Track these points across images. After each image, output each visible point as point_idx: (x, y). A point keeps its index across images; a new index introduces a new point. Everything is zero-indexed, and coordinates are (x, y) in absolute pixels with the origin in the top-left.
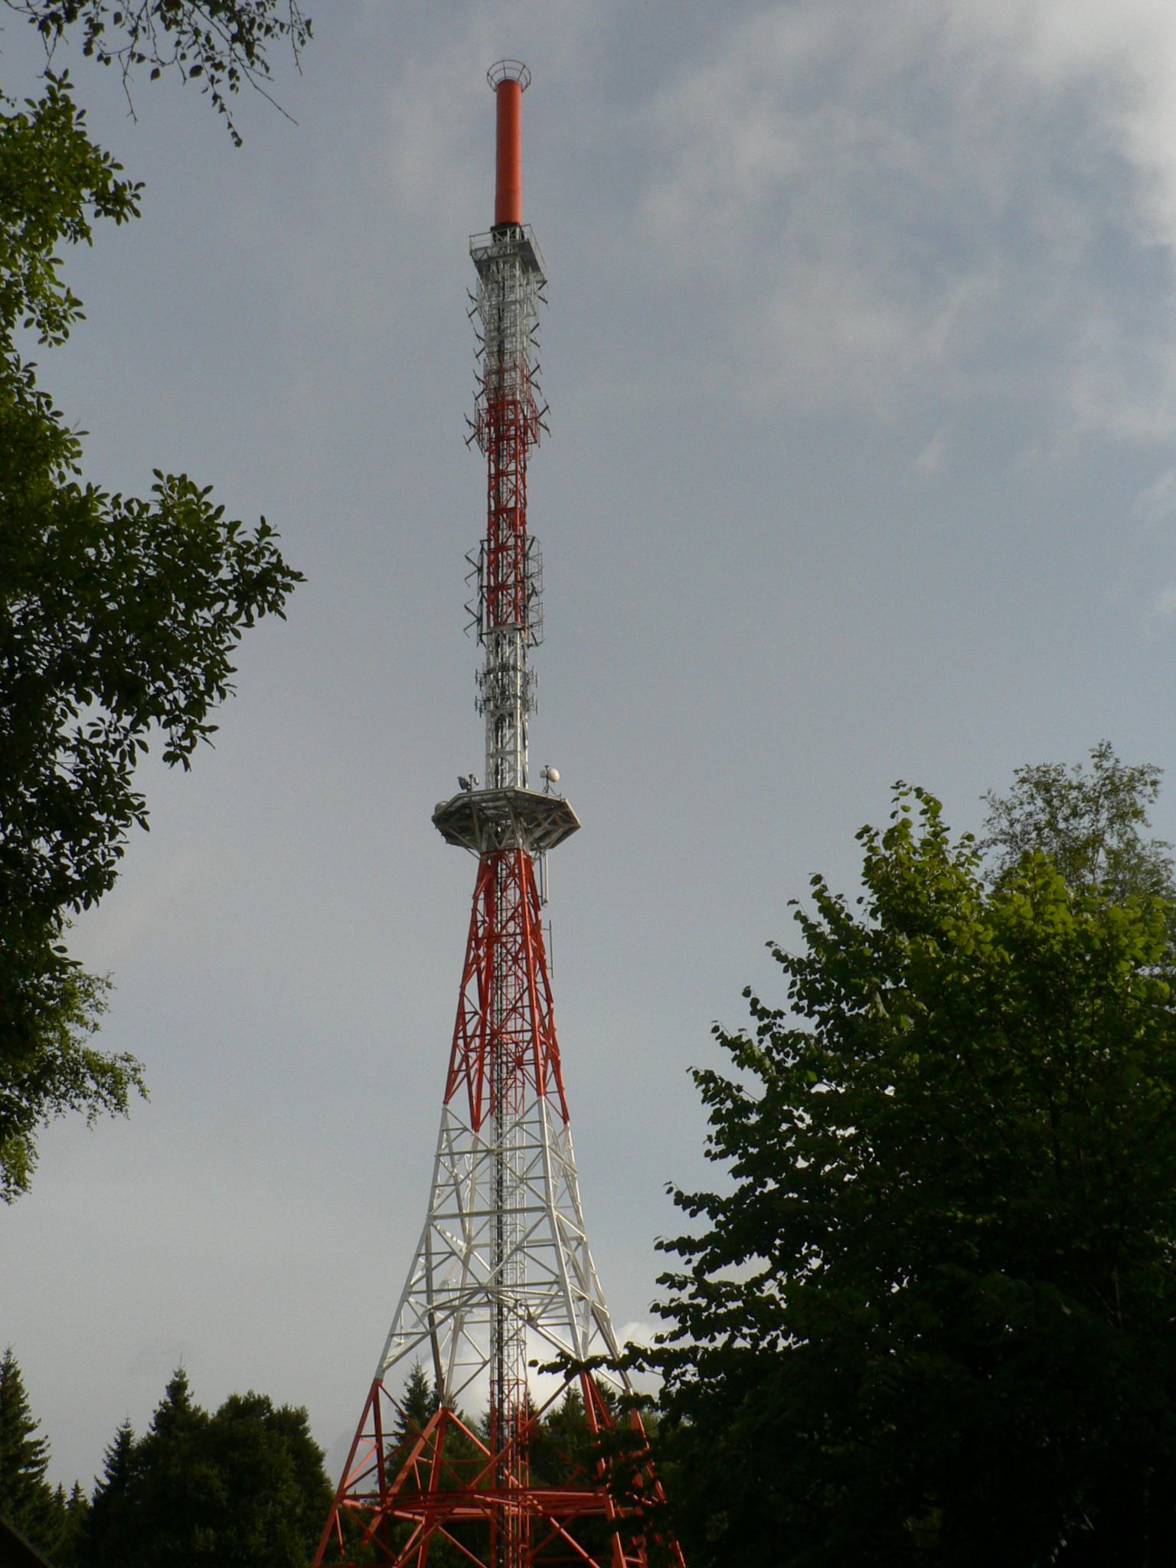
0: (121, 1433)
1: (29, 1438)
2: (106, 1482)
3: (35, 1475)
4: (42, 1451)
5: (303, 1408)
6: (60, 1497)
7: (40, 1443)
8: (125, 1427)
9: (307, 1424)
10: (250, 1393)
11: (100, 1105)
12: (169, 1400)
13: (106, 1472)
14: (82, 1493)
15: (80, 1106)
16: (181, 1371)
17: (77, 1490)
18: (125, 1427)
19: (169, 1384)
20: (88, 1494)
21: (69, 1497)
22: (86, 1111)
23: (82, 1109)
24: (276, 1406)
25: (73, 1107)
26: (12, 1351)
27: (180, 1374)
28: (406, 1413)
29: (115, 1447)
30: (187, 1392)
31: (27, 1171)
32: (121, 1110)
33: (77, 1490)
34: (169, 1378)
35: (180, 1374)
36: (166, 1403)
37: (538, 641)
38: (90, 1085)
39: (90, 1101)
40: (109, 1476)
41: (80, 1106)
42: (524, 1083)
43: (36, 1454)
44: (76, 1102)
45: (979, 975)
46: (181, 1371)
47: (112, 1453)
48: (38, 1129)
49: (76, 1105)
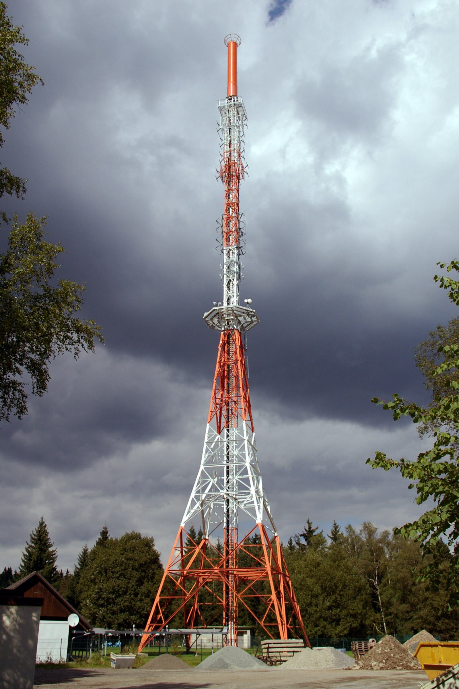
0: (84, 549)
1: (51, 549)
2: (79, 567)
3: (52, 562)
4: (54, 554)
5: (152, 537)
6: (62, 574)
7: (54, 551)
8: (85, 547)
9: (154, 543)
10: (133, 532)
11: (80, 348)
12: (101, 537)
13: (79, 563)
14: (69, 573)
15: (71, 349)
16: (105, 527)
17: (68, 572)
18: (85, 547)
19: (101, 531)
20: (72, 572)
21: (65, 574)
22: (73, 350)
23: (71, 350)
24: (142, 537)
25: (67, 349)
26: (43, 517)
27: (105, 528)
28: (188, 543)
29: (82, 554)
30: (108, 535)
31: (47, 381)
32: (91, 349)
33: (68, 572)
34: (101, 529)
35: (105, 528)
36: (100, 538)
37: (244, 253)
38: (75, 336)
39: (76, 346)
40: (80, 565)
41: (71, 349)
42: (237, 417)
43: (52, 555)
44: (69, 347)
45: (211, 591)
46: (105, 527)
47: (80, 556)
48: (51, 358)
49: (69, 349)
